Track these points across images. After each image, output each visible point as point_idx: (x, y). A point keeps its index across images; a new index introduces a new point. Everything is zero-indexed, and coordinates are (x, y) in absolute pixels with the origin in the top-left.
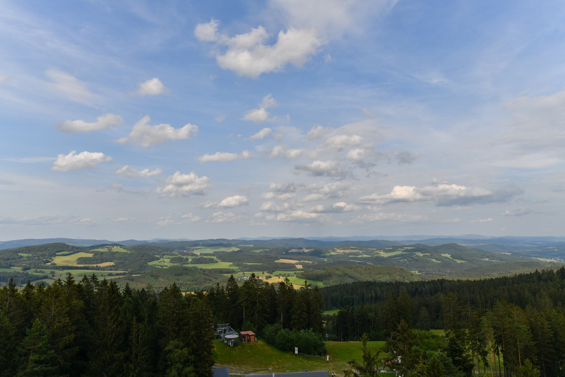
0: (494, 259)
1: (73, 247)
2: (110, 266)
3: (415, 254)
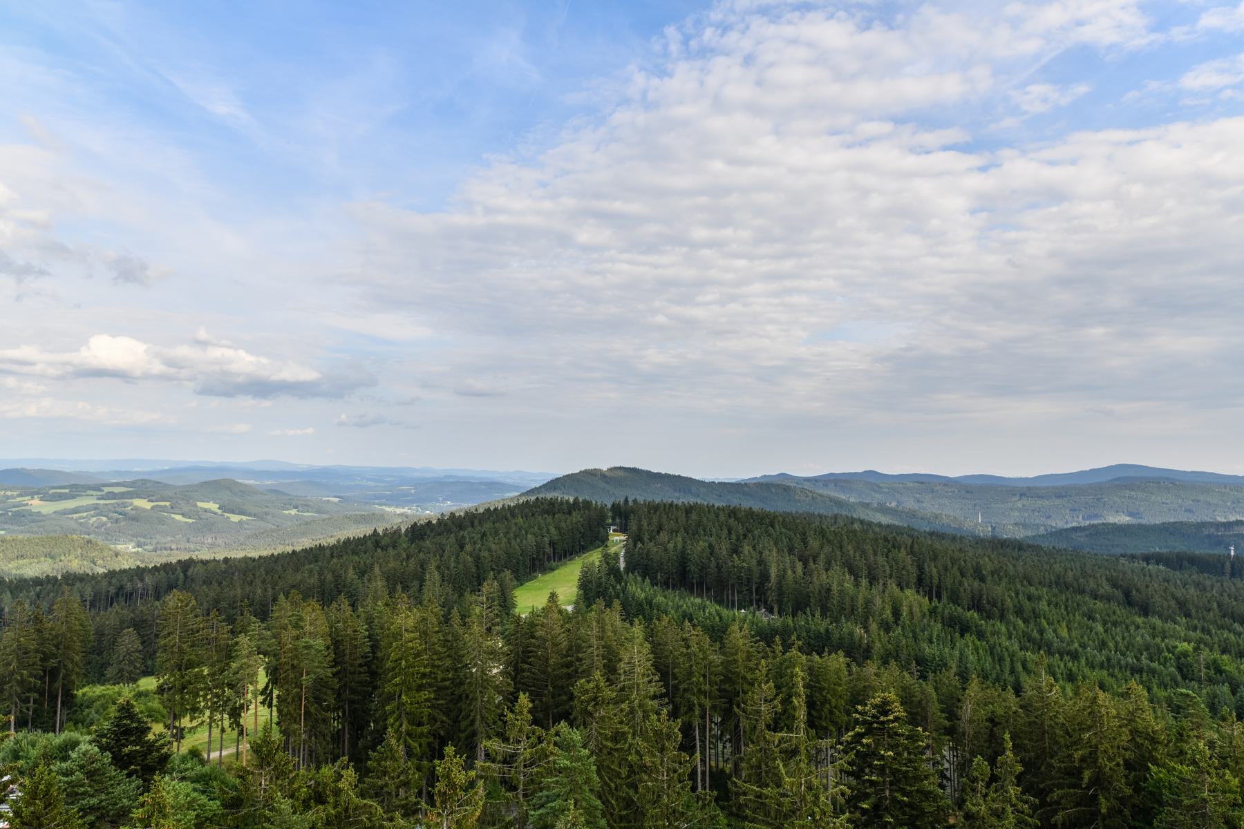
0: (308, 512)
3: (131, 504)
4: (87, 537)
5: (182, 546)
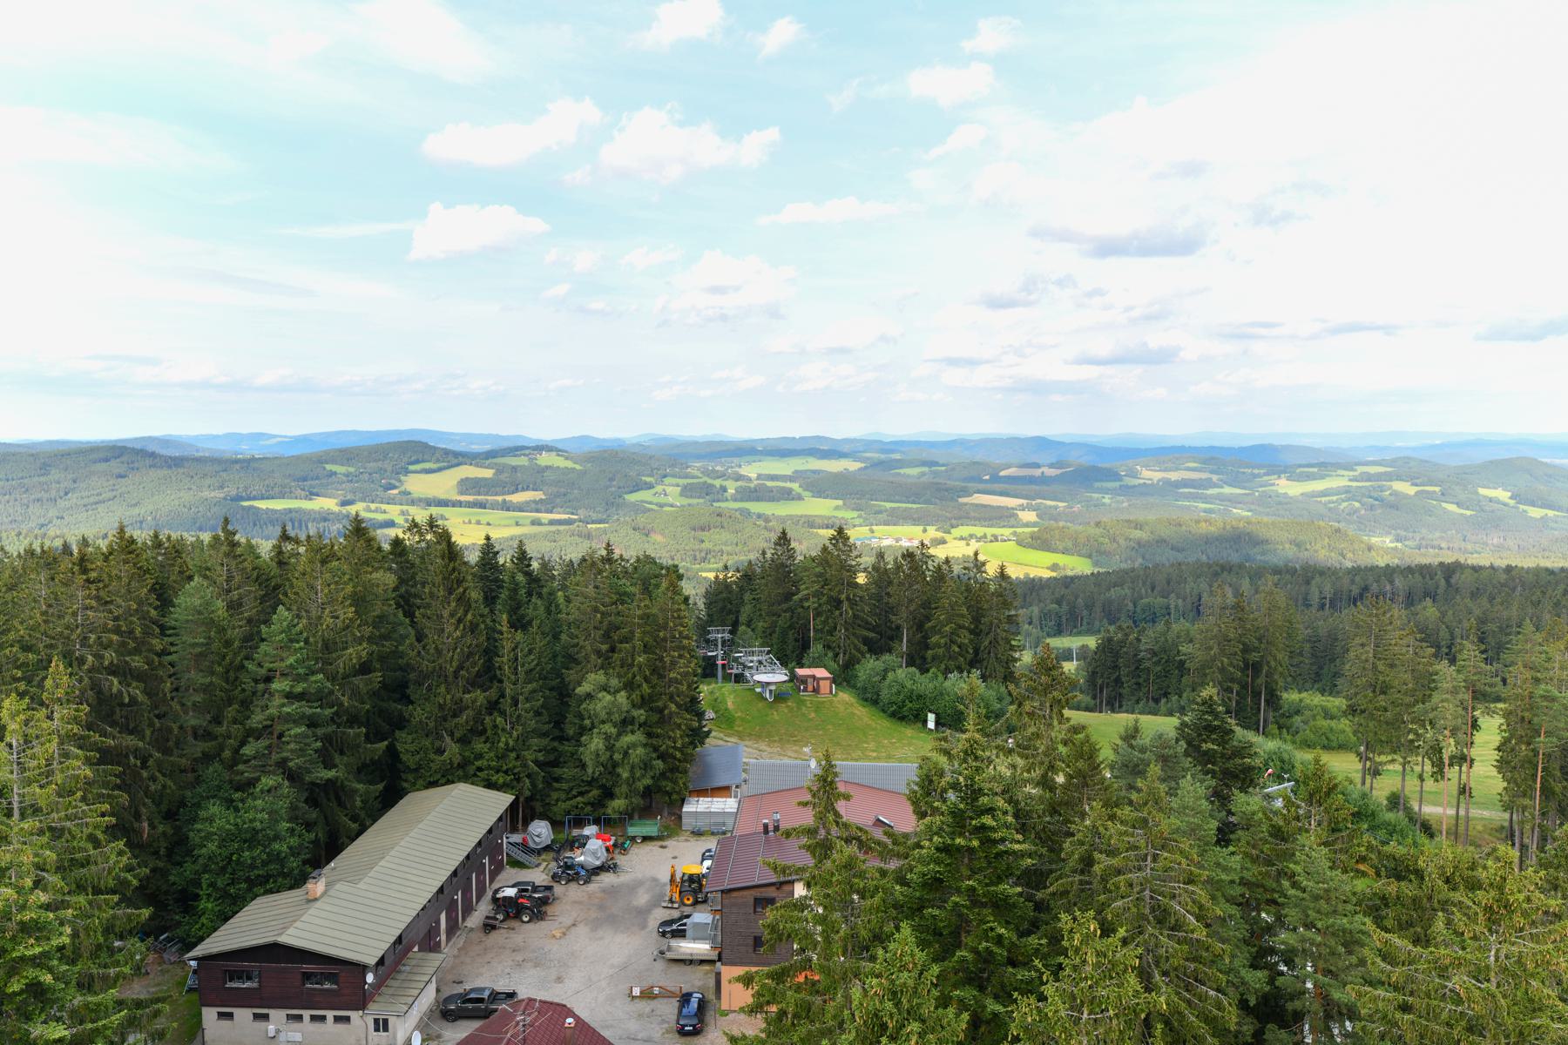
1: (447, 452)
2: (535, 502)
3: (1390, 488)
4: (1337, 524)
5: (1456, 546)
